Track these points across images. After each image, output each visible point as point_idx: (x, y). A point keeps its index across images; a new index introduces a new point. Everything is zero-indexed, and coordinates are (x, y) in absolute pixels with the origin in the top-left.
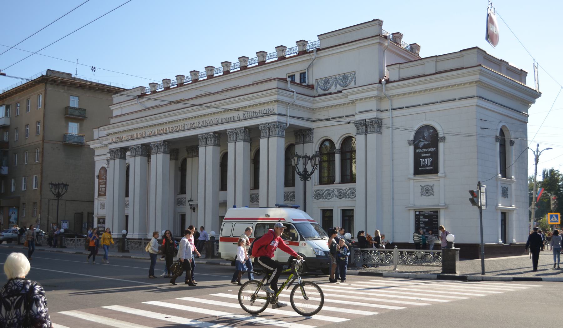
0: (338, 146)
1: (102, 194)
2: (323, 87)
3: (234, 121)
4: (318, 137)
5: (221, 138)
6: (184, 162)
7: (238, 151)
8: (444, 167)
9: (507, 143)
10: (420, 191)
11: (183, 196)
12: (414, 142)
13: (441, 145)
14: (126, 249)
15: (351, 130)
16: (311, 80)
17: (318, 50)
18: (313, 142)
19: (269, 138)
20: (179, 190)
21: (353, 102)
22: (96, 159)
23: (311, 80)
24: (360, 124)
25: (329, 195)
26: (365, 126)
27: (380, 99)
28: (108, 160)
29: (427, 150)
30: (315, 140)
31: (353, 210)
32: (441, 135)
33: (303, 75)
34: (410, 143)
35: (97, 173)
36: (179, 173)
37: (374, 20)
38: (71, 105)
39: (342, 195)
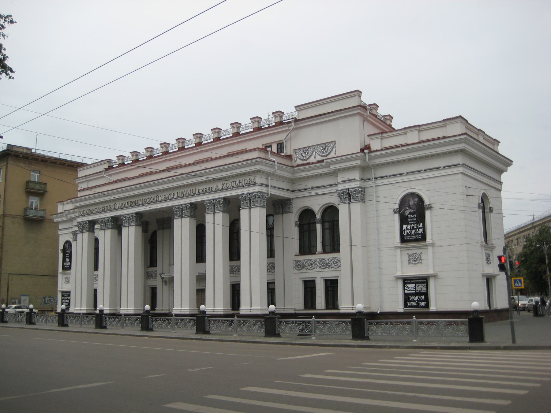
0: (318, 216)
2: (302, 158)
3: (211, 191)
4: (297, 206)
5: (197, 211)
6: (154, 234)
8: (432, 234)
9: (487, 210)
10: (408, 259)
13: (428, 213)
14: (104, 324)
15: (334, 200)
16: (288, 150)
17: (296, 120)
18: (292, 212)
19: (214, 214)
20: (149, 263)
21: (335, 173)
22: (60, 233)
23: (288, 150)
24: (343, 193)
25: (312, 264)
26: (348, 196)
27: (364, 169)
28: (75, 234)
32: (427, 202)
33: (280, 145)
34: (395, 211)
36: (149, 246)
38: (32, 179)
39: (325, 265)
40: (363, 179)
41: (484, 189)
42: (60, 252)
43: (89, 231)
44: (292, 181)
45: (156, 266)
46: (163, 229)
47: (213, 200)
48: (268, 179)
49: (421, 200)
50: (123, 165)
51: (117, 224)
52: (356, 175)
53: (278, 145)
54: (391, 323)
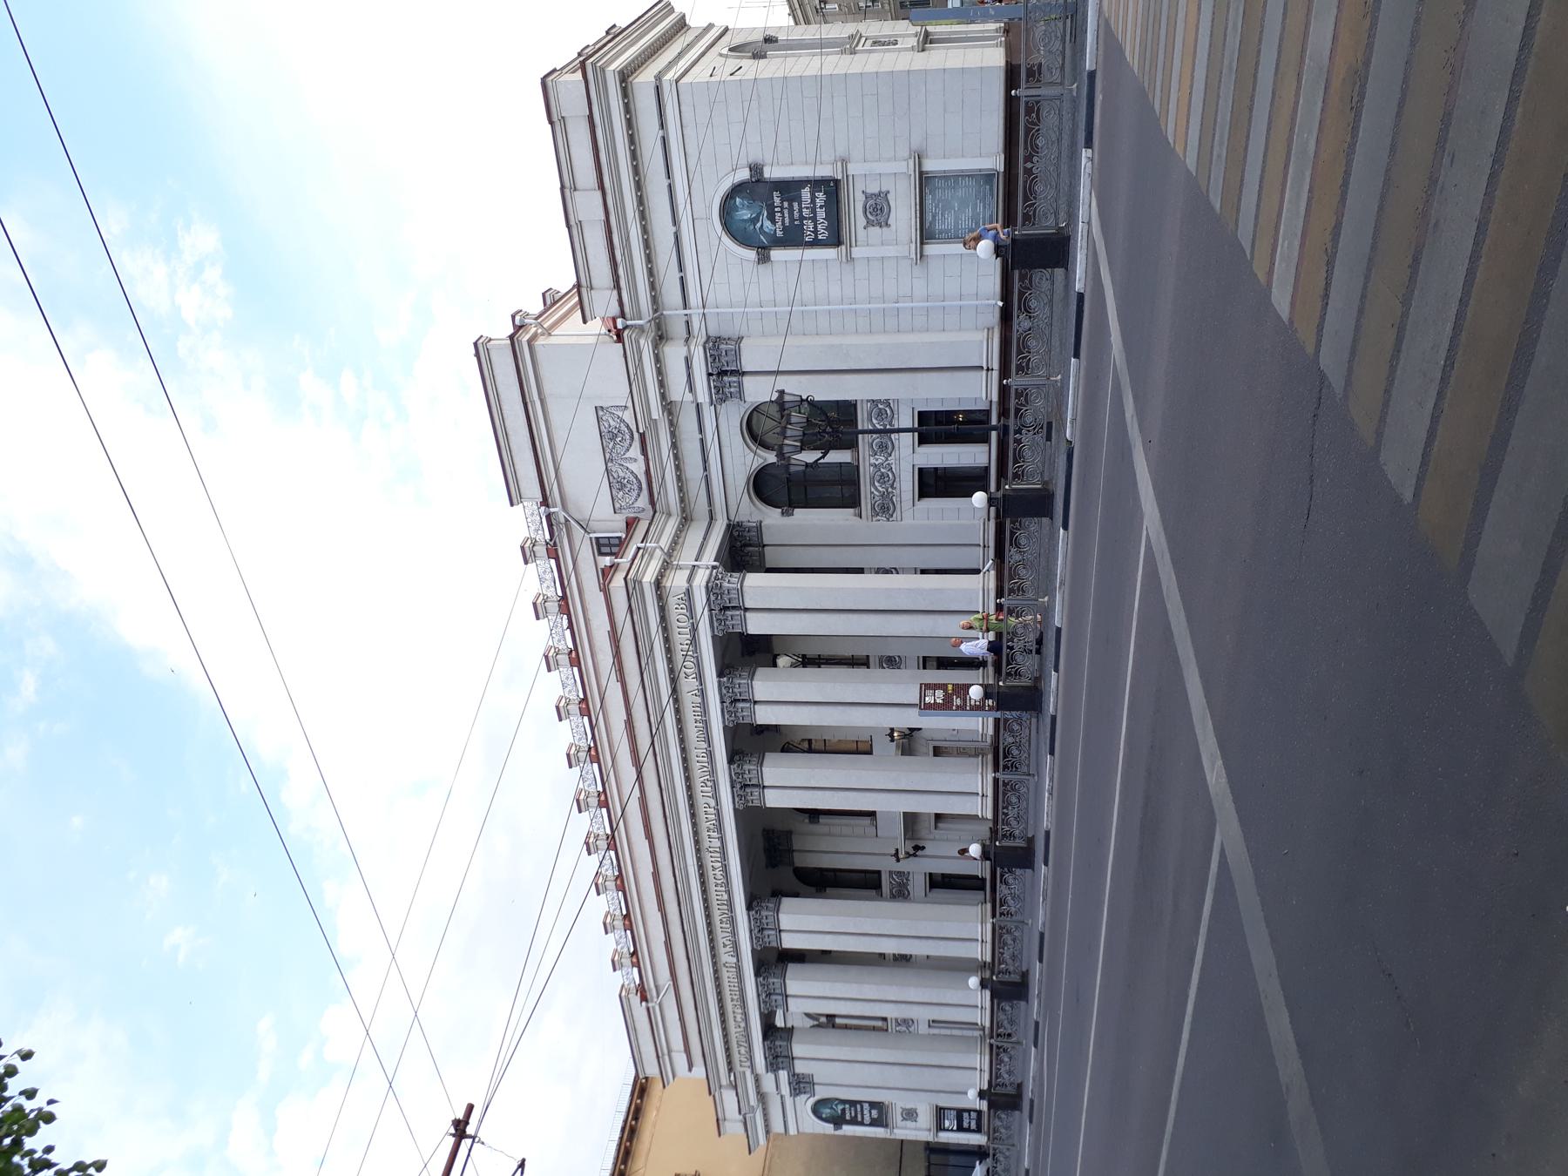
1: (881, 1114)
2: (635, 494)
5: (751, 742)
7: (779, 696)
11: (885, 879)
12: (764, 248)
13: (770, 173)
15: (733, 416)
17: (545, 502)
19: (746, 610)
20: (873, 892)
21: (669, 407)
23: (616, 528)
25: (886, 478)
26: (725, 371)
28: (800, 1084)
29: (781, 212)
30: (756, 518)
31: (920, 470)
32: (744, 175)
33: (604, 546)
35: (828, 1128)
37: (477, 354)
40: (687, 340)
41: (723, 47)
42: (838, 1132)
43: (789, 1039)
44: (686, 519)
45: (879, 872)
46: (791, 851)
47: (722, 702)
48: (679, 567)
49: (737, 190)
50: (612, 843)
51: (774, 960)
52: (674, 354)
53: (601, 554)
54: (1028, 159)
